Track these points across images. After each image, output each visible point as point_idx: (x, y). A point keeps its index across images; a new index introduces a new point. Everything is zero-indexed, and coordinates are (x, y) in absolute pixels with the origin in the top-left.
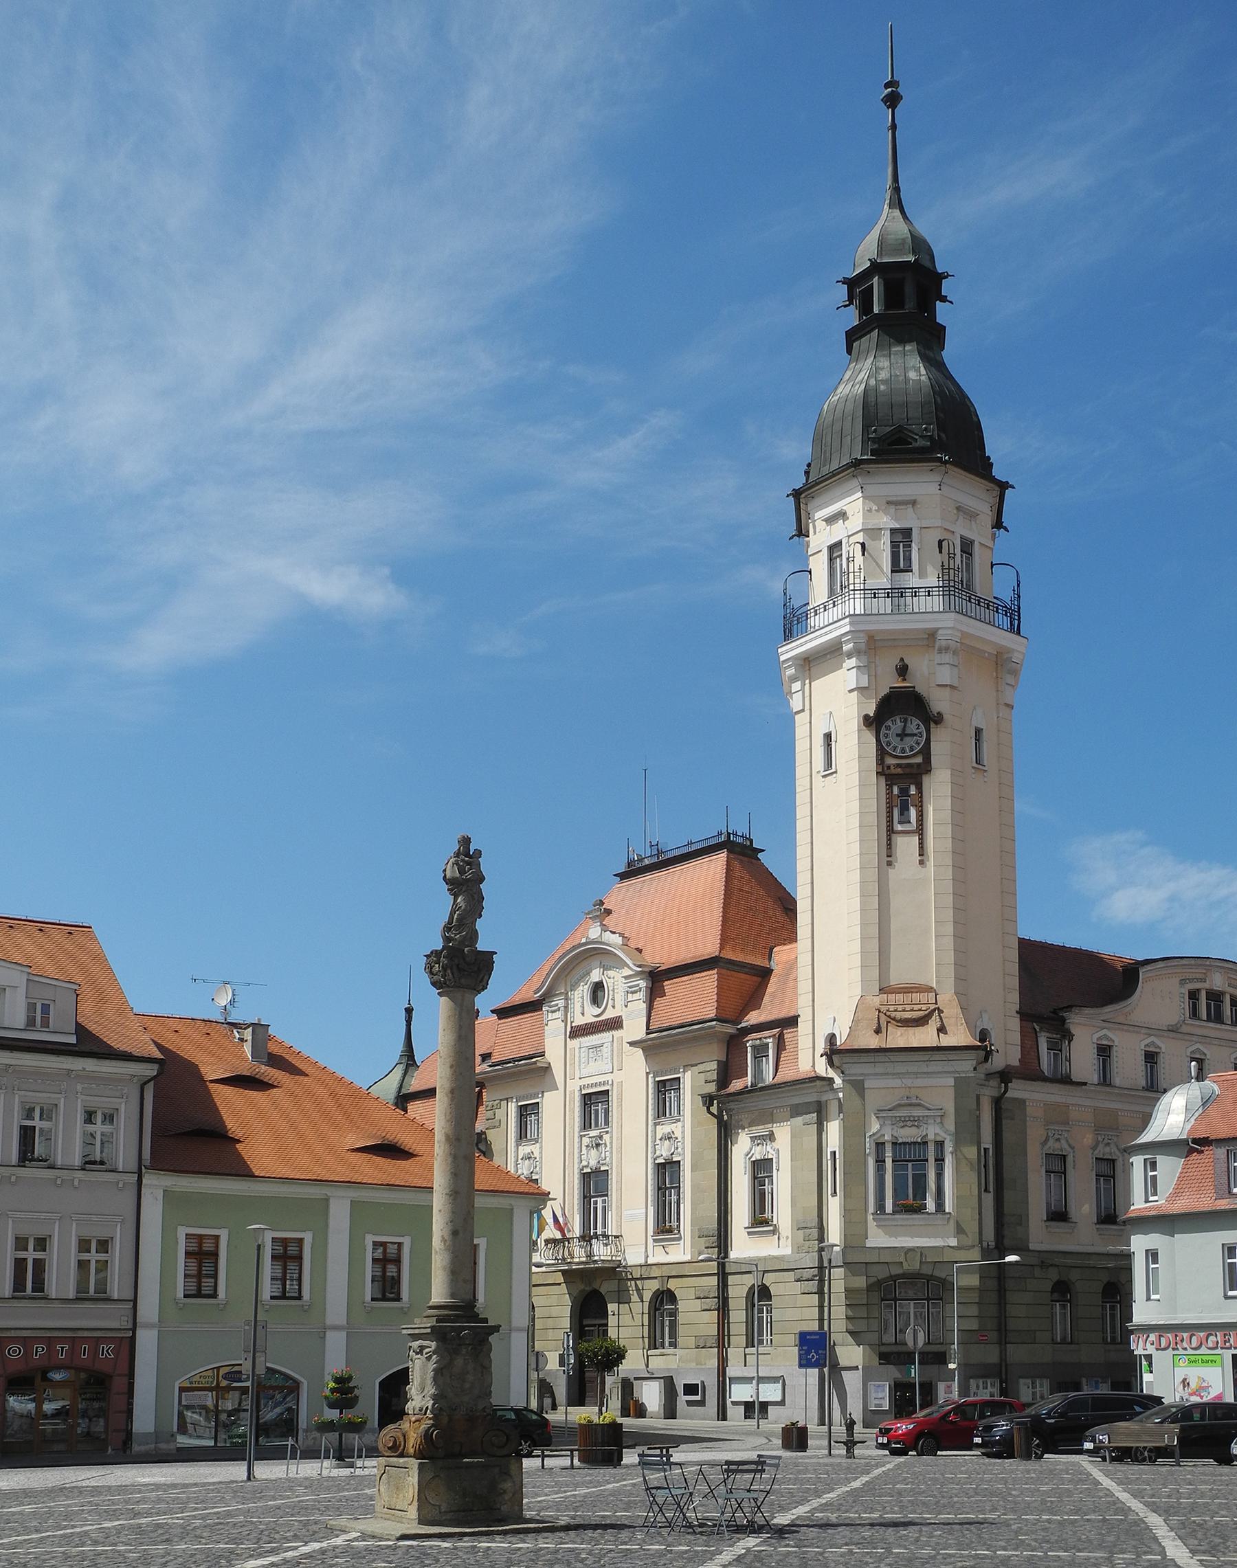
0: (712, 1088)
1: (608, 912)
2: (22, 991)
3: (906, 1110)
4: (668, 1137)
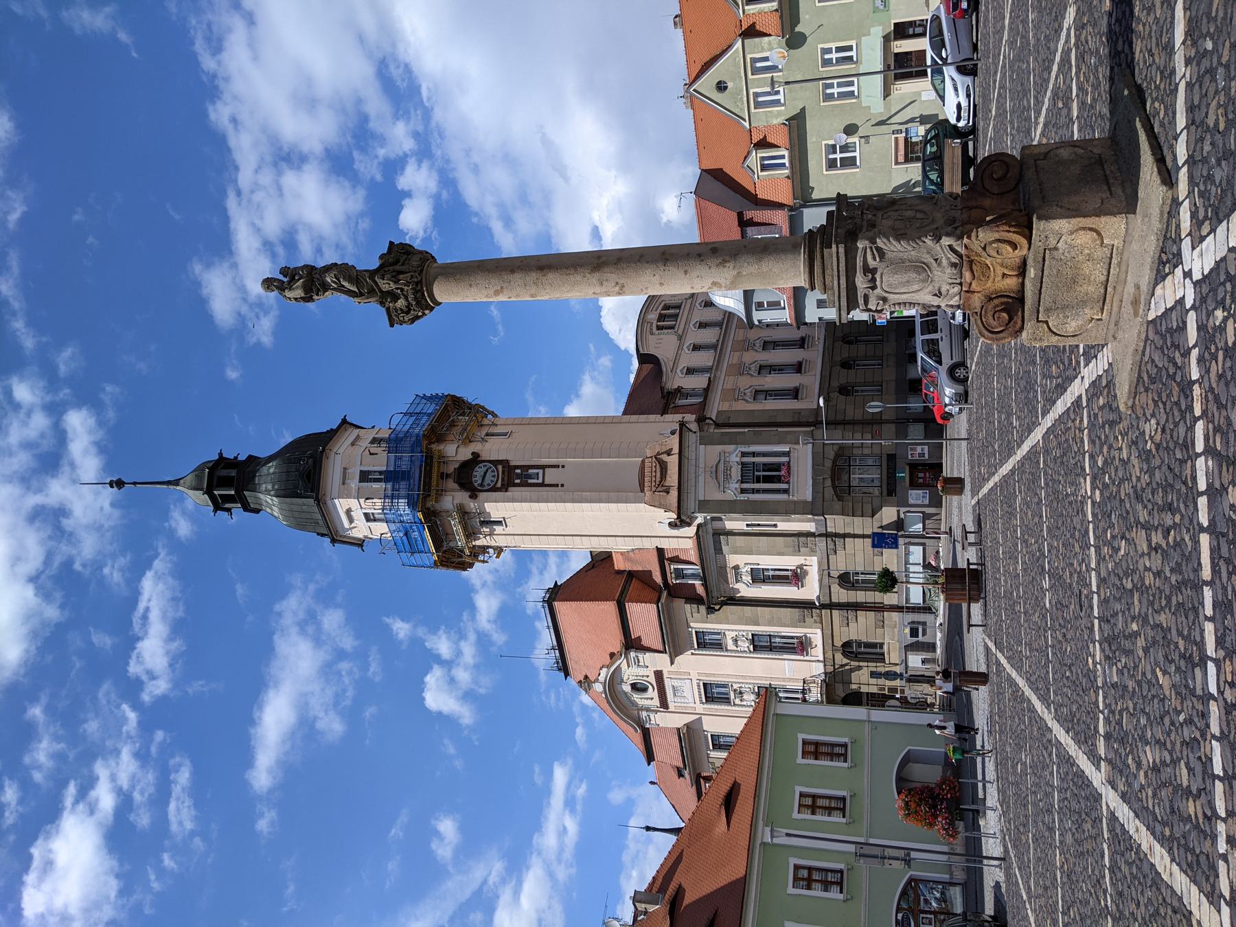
0: (703, 608)
1: (586, 677)
3: (719, 473)
4: (735, 641)
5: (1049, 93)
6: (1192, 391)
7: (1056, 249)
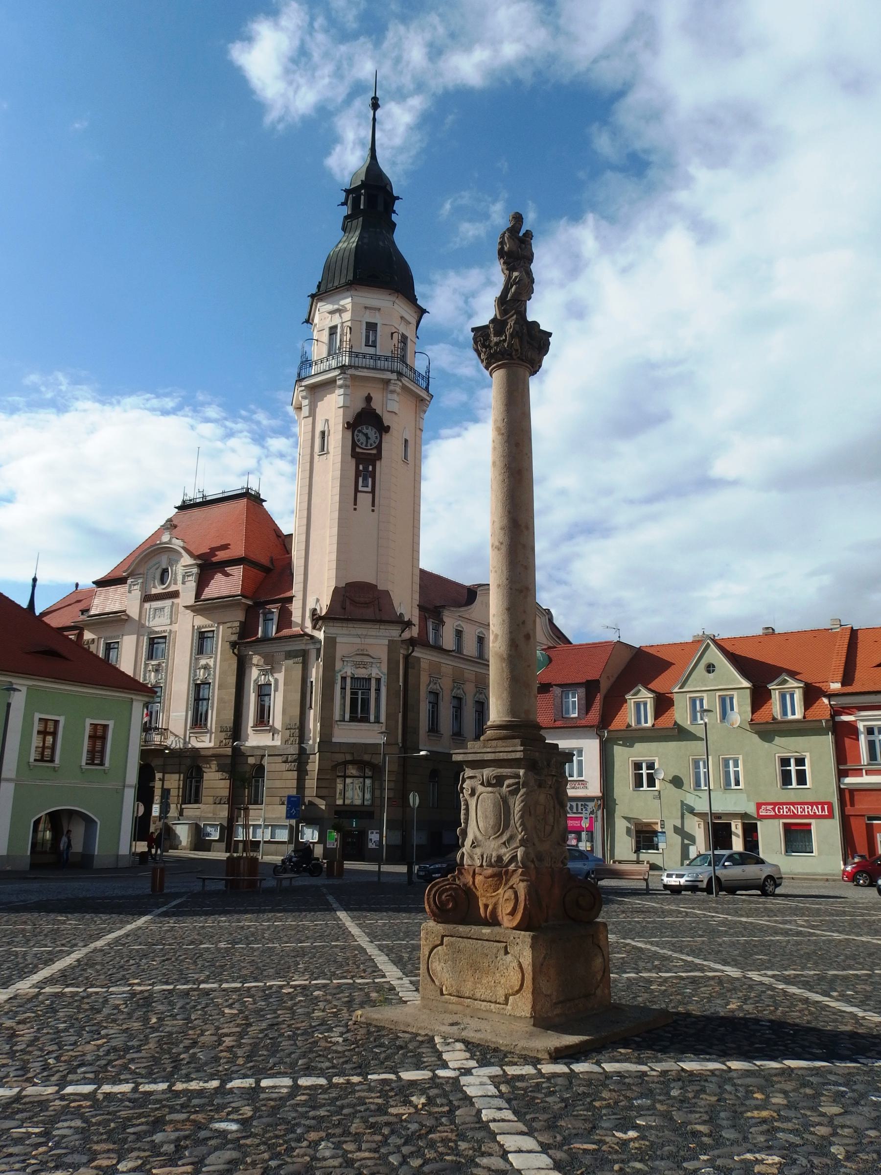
0: (234, 638)
5: (670, 953)
6: (358, 1075)
7: (507, 953)
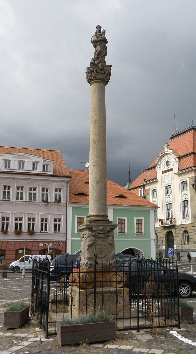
2: (42, 163)
4: (184, 195)
